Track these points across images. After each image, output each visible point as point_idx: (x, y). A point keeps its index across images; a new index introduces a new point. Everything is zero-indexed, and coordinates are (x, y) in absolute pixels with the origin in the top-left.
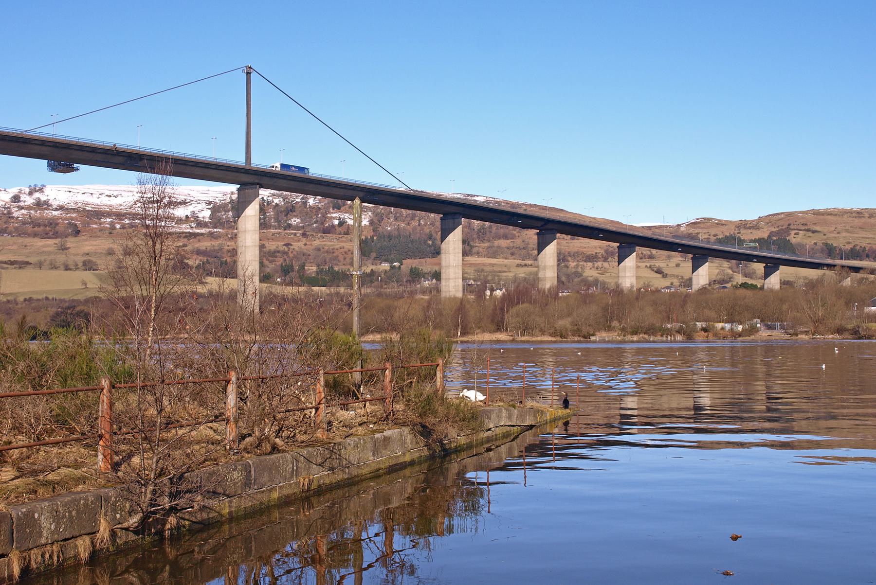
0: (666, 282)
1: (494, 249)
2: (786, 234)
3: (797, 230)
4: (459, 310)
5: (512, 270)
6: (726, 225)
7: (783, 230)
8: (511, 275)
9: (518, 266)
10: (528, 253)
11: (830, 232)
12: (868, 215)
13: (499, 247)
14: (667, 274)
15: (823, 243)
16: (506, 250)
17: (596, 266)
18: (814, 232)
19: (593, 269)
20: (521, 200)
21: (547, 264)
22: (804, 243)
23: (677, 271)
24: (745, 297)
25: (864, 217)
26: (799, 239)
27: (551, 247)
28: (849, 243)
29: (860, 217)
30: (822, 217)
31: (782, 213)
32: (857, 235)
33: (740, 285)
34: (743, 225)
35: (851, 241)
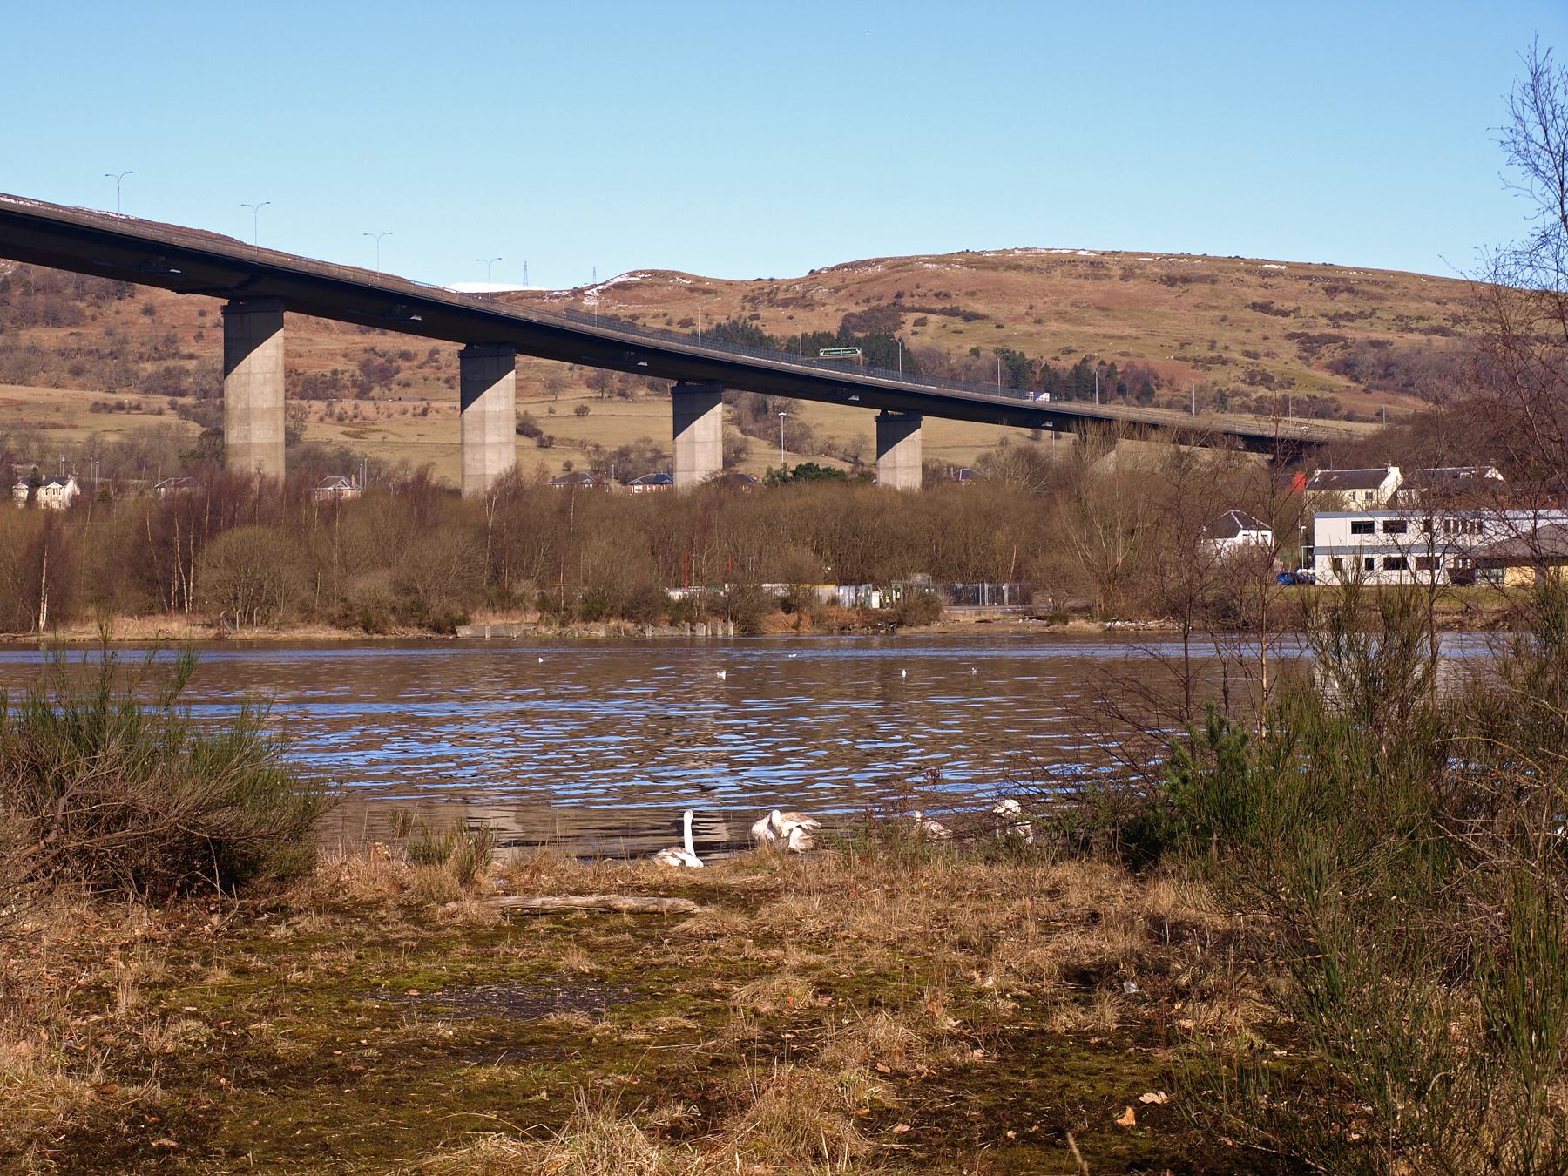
0: (554, 464)
1: (21, 355)
2: (890, 323)
3: (922, 310)
4: (41, 546)
5: (78, 422)
6: (716, 293)
7: (879, 309)
8: (80, 436)
9: (97, 408)
10: (126, 371)
11: (1014, 320)
12: (1120, 272)
13: (33, 350)
14: (551, 438)
15: (996, 352)
16: (56, 358)
17: (337, 410)
18: (970, 317)
19: (327, 420)
20: (136, 213)
21: (253, 404)
22: (944, 351)
23: (577, 430)
24: (883, 509)
25: (1110, 277)
26: (927, 338)
27: (267, 352)
28: (1068, 351)
29: (1097, 277)
30: (992, 274)
31: (878, 261)
32: (1091, 330)
33: (795, 473)
34: (766, 293)
35: (1074, 346)
